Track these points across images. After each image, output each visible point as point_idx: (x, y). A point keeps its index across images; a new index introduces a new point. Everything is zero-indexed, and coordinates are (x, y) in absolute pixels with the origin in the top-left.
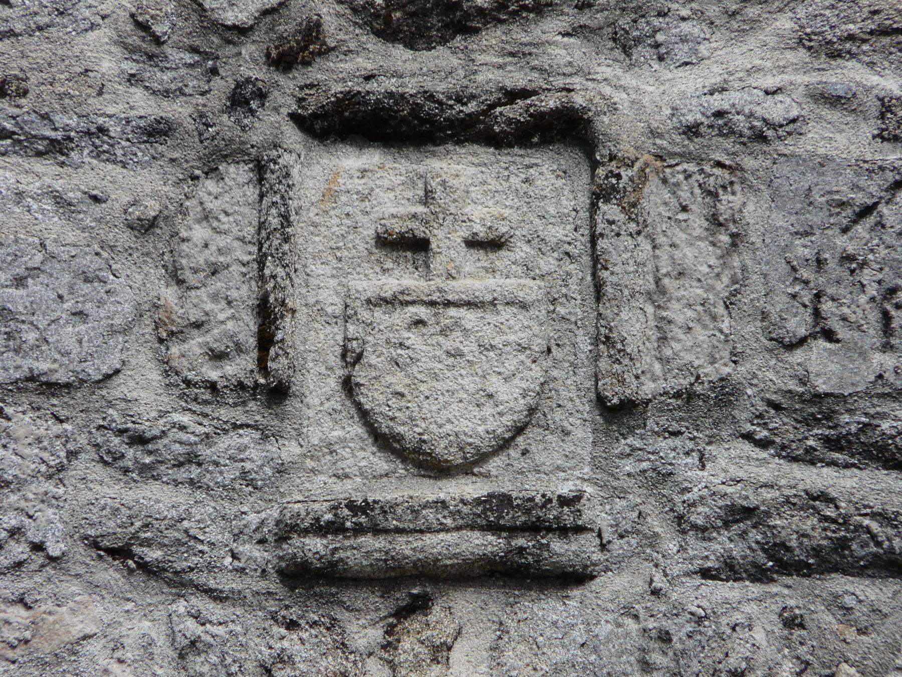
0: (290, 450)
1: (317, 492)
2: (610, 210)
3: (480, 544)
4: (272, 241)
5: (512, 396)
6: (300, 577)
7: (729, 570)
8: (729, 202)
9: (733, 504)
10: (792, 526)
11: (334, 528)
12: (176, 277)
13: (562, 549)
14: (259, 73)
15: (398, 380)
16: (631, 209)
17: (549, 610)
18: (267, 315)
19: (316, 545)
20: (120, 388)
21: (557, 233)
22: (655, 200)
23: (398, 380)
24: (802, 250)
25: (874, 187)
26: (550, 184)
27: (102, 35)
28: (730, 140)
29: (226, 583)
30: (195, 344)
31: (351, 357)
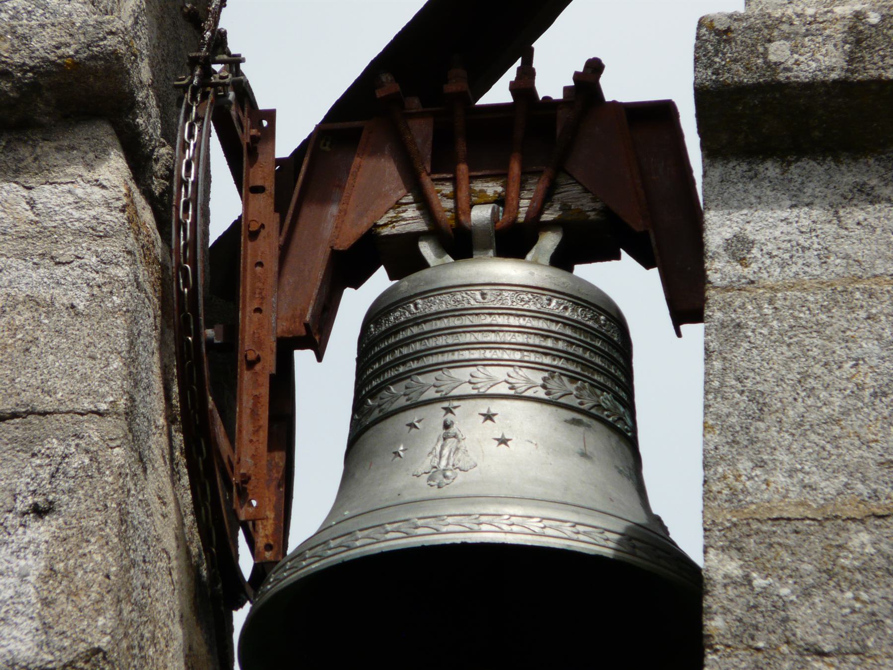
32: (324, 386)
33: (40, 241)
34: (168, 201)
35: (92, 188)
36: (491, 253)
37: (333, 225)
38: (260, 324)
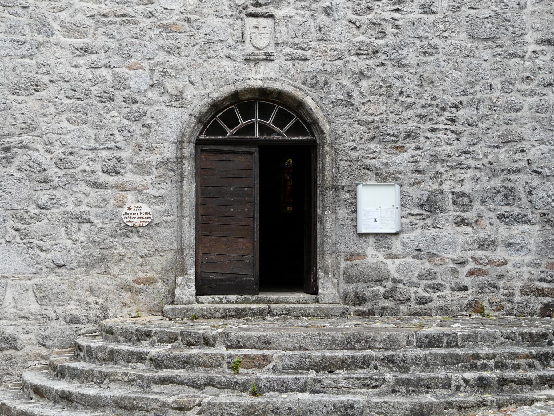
0: (245, 47)
1: (248, 52)
2: (276, 24)
3: (265, 57)
4: (243, 27)
5: (267, 43)
6: (246, 60)
7: (287, 60)
8: (287, 24)
10: (293, 56)
11: (250, 55)
12: (233, 30)
13: (272, 58)
14: (242, 10)
15: (255, 41)
16: (278, 24)
17: (270, 64)
18: (243, 34)
19: (248, 57)
20: (228, 41)
21: (271, 26)
22: (280, 23)
23: (255, 41)
24: (295, 29)
25: (301, 23)
26: (270, 21)
27: (226, 6)
29: (239, 60)
30: (236, 37)
31: (251, 38)
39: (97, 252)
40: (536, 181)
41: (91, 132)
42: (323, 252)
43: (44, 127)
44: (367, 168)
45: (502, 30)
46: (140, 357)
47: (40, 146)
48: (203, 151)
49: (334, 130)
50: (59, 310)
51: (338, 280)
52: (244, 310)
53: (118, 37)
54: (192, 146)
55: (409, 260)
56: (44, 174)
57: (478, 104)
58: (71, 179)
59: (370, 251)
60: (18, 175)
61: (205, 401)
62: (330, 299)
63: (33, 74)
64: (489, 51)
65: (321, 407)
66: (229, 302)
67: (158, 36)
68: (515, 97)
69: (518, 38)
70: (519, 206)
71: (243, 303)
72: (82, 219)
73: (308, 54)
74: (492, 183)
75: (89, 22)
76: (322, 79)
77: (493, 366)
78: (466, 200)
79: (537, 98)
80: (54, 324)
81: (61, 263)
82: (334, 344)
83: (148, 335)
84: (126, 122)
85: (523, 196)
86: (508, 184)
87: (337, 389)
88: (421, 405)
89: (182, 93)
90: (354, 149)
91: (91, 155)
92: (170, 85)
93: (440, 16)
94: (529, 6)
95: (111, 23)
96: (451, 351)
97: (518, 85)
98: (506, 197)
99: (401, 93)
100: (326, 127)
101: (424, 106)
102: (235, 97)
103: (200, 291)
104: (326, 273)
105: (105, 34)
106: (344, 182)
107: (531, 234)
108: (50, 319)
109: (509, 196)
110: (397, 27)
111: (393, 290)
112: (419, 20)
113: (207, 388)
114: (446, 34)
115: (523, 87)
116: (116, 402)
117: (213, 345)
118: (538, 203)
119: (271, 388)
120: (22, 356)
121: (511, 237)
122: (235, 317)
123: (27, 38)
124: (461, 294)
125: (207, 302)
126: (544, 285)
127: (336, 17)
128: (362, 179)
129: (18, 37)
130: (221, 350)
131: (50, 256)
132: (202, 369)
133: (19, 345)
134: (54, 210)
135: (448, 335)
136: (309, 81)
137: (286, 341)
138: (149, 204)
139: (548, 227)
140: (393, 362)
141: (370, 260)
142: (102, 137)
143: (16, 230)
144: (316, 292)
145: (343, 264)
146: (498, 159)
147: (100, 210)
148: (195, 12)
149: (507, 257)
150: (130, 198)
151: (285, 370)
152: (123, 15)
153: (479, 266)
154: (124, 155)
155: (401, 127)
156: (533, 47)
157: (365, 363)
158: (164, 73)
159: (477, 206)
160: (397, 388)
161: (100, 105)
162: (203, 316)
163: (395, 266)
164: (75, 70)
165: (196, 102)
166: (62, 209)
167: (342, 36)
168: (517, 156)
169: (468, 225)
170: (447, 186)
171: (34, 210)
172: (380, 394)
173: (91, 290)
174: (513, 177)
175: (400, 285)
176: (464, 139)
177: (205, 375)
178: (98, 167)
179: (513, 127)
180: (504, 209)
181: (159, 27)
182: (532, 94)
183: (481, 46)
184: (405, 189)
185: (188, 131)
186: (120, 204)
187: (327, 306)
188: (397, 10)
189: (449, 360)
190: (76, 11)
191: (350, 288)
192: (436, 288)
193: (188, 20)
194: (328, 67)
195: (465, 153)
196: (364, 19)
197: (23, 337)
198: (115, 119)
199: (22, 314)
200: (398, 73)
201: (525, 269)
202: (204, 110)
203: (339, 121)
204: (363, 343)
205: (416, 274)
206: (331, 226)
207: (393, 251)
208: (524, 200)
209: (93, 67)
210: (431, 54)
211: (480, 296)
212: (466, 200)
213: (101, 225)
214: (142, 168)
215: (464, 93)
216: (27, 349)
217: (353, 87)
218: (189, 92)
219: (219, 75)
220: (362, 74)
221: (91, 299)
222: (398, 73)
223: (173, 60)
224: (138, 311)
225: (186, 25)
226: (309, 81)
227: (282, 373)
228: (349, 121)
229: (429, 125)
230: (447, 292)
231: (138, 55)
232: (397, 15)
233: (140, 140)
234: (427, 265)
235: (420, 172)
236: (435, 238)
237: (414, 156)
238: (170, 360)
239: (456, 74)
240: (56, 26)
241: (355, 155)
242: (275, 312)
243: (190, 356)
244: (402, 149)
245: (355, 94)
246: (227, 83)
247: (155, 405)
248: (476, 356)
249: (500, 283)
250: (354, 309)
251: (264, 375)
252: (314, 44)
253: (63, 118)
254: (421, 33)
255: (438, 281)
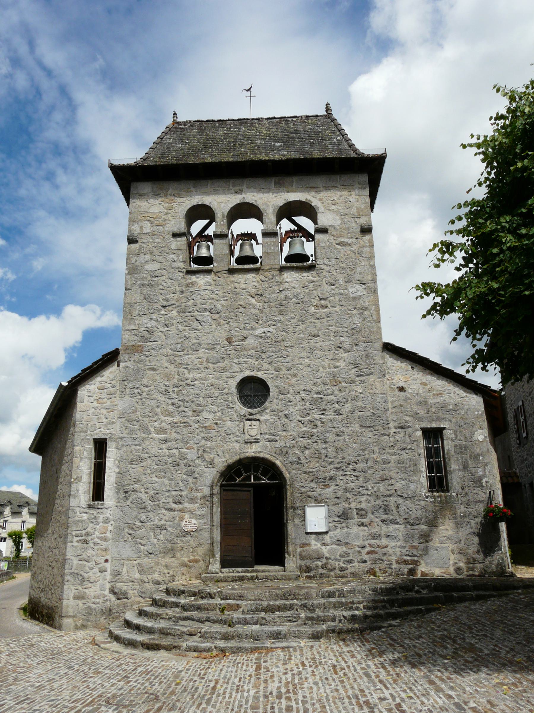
1: (246, 438)
4: (244, 426)
9: (478, 535)
26: (258, 422)
28: (266, 420)
32: (195, 248)
33: (182, 241)
34: (188, 239)
35: (184, 238)
36: (321, 189)
37: (196, 241)
38: (192, 245)
39: (169, 546)
40: (400, 501)
41: (167, 482)
42: (287, 543)
43: (145, 480)
44: (310, 497)
45: (377, 422)
46: (177, 605)
47: (142, 490)
48: (224, 490)
49: (292, 477)
50: (150, 577)
51: (296, 558)
52: (243, 577)
53: (182, 433)
54: (218, 488)
55: (334, 546)
56: (144, 504)
57: (367, 461)
58: (157, 507)
59: (313, 542)
60: (131, 506)
61: (203, 630)
62: (291, 570)
63: (140, 454)
64: (371, 433)
65: (263, 633)
66: (238, 572)
67: (201, 432)
68: (386, 456)
69: (385, 426)
70: (392, 515)
71: (245, 572)
72: (162, 528)
73: (277, 438)
74: (377, 503)
75: (168, 427)
76: (284, 451)
77: (362, 608)
78: (364, 512)
79: (398, 456)
80: (147, 585)
81: (151, 552)
82: (277, 597)
83: (183, 592)
84: (185, 476)
85: (394, 509)
86: (385, 503)
87: (274, 623)
88: (317, 632)
89: (213, 460)
90: (303, 487)
91: (167, 494)
92: (207, 456)
93: (345, 416)
94: (390, 409)
95: (178, 427)
96: (339, 599)
97: (388, 450)
98: (385, 510)
99: (326, 456)
100: (287, 475)
101: (339, 463)
102: (240, 462)
103: (223, 566)
104: (289, 555)
105: (176, 432)
106: (298, 505)
107: (399, 530)
108: (145, 582)
109: (386, 509)
110: (323, 423)
111: (326, 564)
112: (334, 419)
113: (207, 623)
114: (348, 425)
115: (390, 451)
116: (160, 630)
117: (214, 598)
118: (402, 513)
119: (239, 623)
120: (130, 602)
121: (389, 532)
122: (239, 581)
123: (138, 436)
124: (363, 565)
125: (227, 572)
126: (408, 558)
127: (291, 419)
128: (307, 502)
129: (134, 436)
130: (218, 601)
131: (146, 548)
132: (206, 612)
133: (129, 597)
134: (148, 524)
135: (339, 591)
136: (278, 452)
137: (252, 596)
138: (196, 519)
139: (408, 526)
140: (306, 607)
141: (313, 547)
142: (173, 484)
143: (130, 534)
144: (284, 566)
145: (299, 550)
146: (379, 489)
147: (171, 523)
148: (220, 419)
149: (387, 543)
150: (187, 516)
151: (249, 612)
152: (185, 423)
153: (373, 549)
154: (184, 493)
155: (327, 474)
156: (394, 430)
157: (291, 607)
158: (204, 451)
159: (370, 515)
160: (307, 622)
161: (172, 468)
162: (221, 580)
163: (326, 550)
164: (160, 451)
165: (220, 465)
166: (152, 523)
167: (295, 428)
168: (390, 488)
169: (366, 526)
170: (353, 505)
171: (138, 524)
172: (298, 626)
173: (166, 567)
174: (388, 499)
175: (330, 561)
176: (361, 479)
177: (204, 615)
178: (171, 500)
179: (386, 472)
180: (384, 517)
181: (202, 427)
182: (395, 454)
183: (367, 430)
184: (330, 507)
185: (216, 480)
186: (181, 519)
187: (289, 573)
188: (323, 414)
189: (337, 605)
190: (162, 421)
191: (303, 563)
192: (350, 562)
193: (216, 424)
194: (288, 445)
195: (362, 487)
196: (306, 419)
197: (131, 592)
198: (180, 475)
199: (131, 579)
200: (324, 446)
201: (398, 549)
202: (224, 469)
203: (294, 472)
204: (292, 596)
205: (338, 554)
206: (292, 529)
207: (325, 542)
208: (395, 511)
209: (169, 449)
210: (341, 436)
211: (374, 566)
212: (364, 512)
213: (172, 531)
214: (192, 500)
215: (359, 455)
216: (133, 598)
217: (301, 454)
218: (216, 460)
219: (232, 451)
220: (305, 447)
221: (166, 571)
222: (324, 446)
223: (209, 444)
224: (190, 577)
225: (215, 426)
226: (278, 452)
227: (247, 614)
228: (299, 472)
229: (342, 473)
230: (356, 564)
231: (191, 442)
232: (322, 416)
233: (192, 485)
234: (344, 549)
235: (338, 498)
236: (348, 534)
237: (335, 490)
238: (190, 606)
239: (354, 445)
240: (152, 429)
241: (303, 490)
242: (260, 578)
243: (200, 605)
244: (328, 486)
245: (302, 458)
246: (236, 454)
247: (178, 633)
248: (352, 603)
249: (385, 558)
250: (305, 574)
251: (236, 615)
252: (280, 433)
253: (154, 475)
254: (336, 425)
255: (351, 558)
